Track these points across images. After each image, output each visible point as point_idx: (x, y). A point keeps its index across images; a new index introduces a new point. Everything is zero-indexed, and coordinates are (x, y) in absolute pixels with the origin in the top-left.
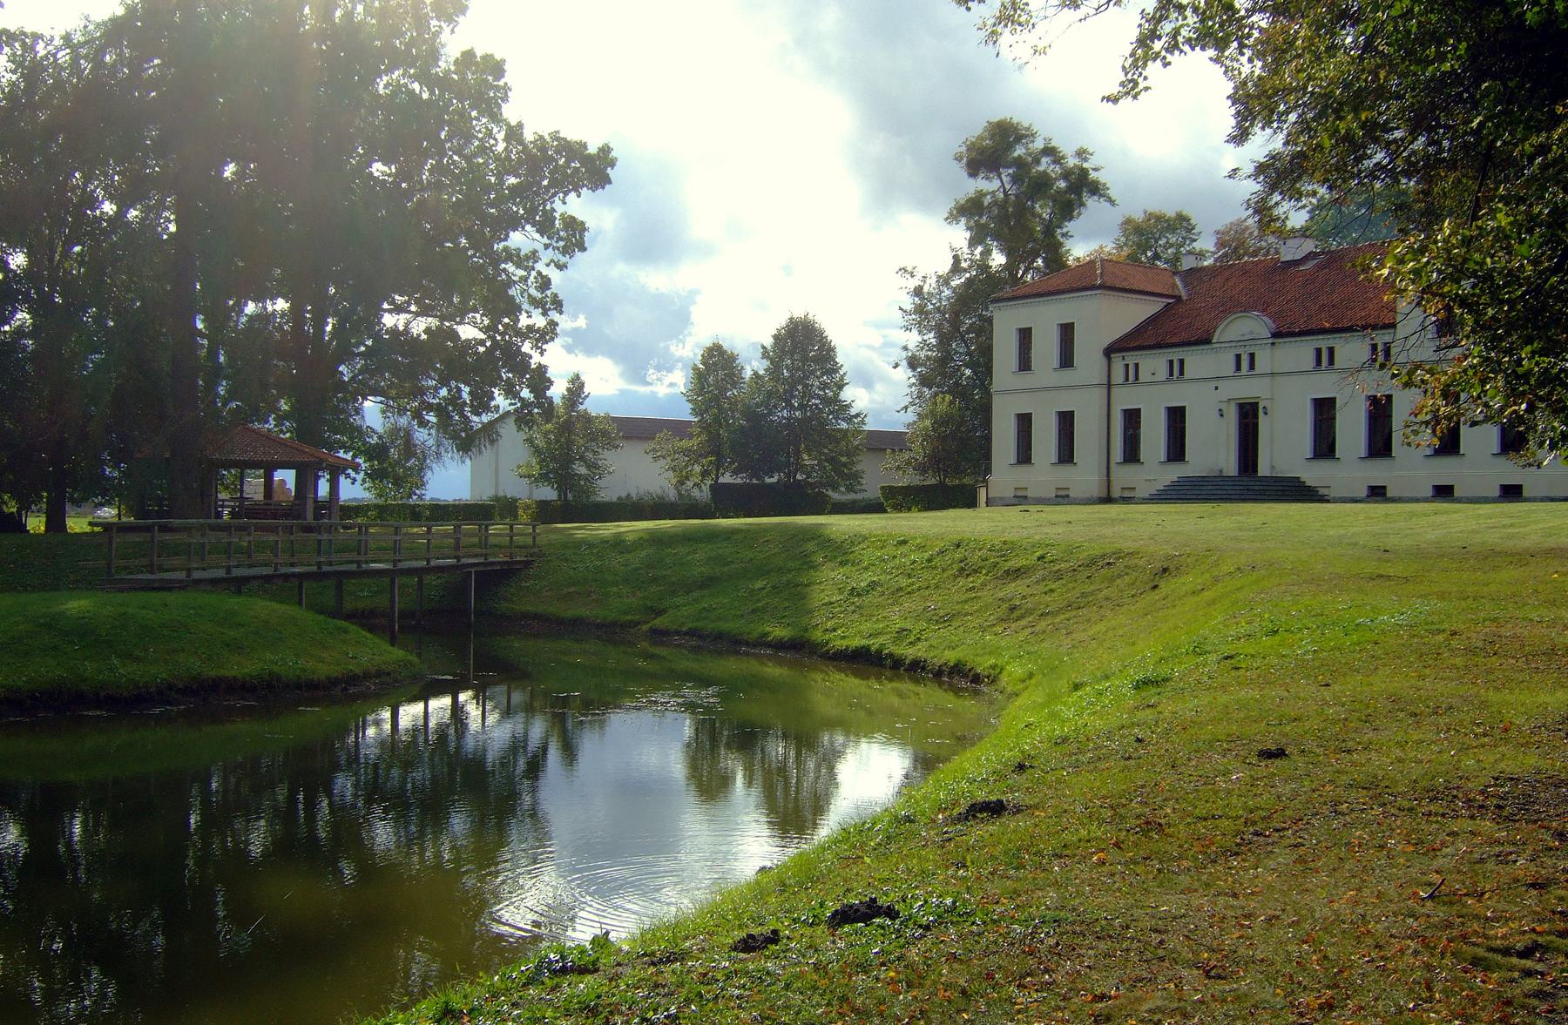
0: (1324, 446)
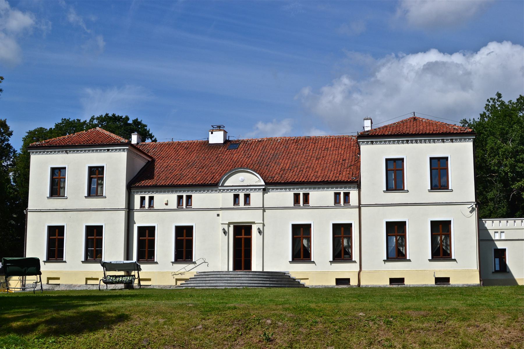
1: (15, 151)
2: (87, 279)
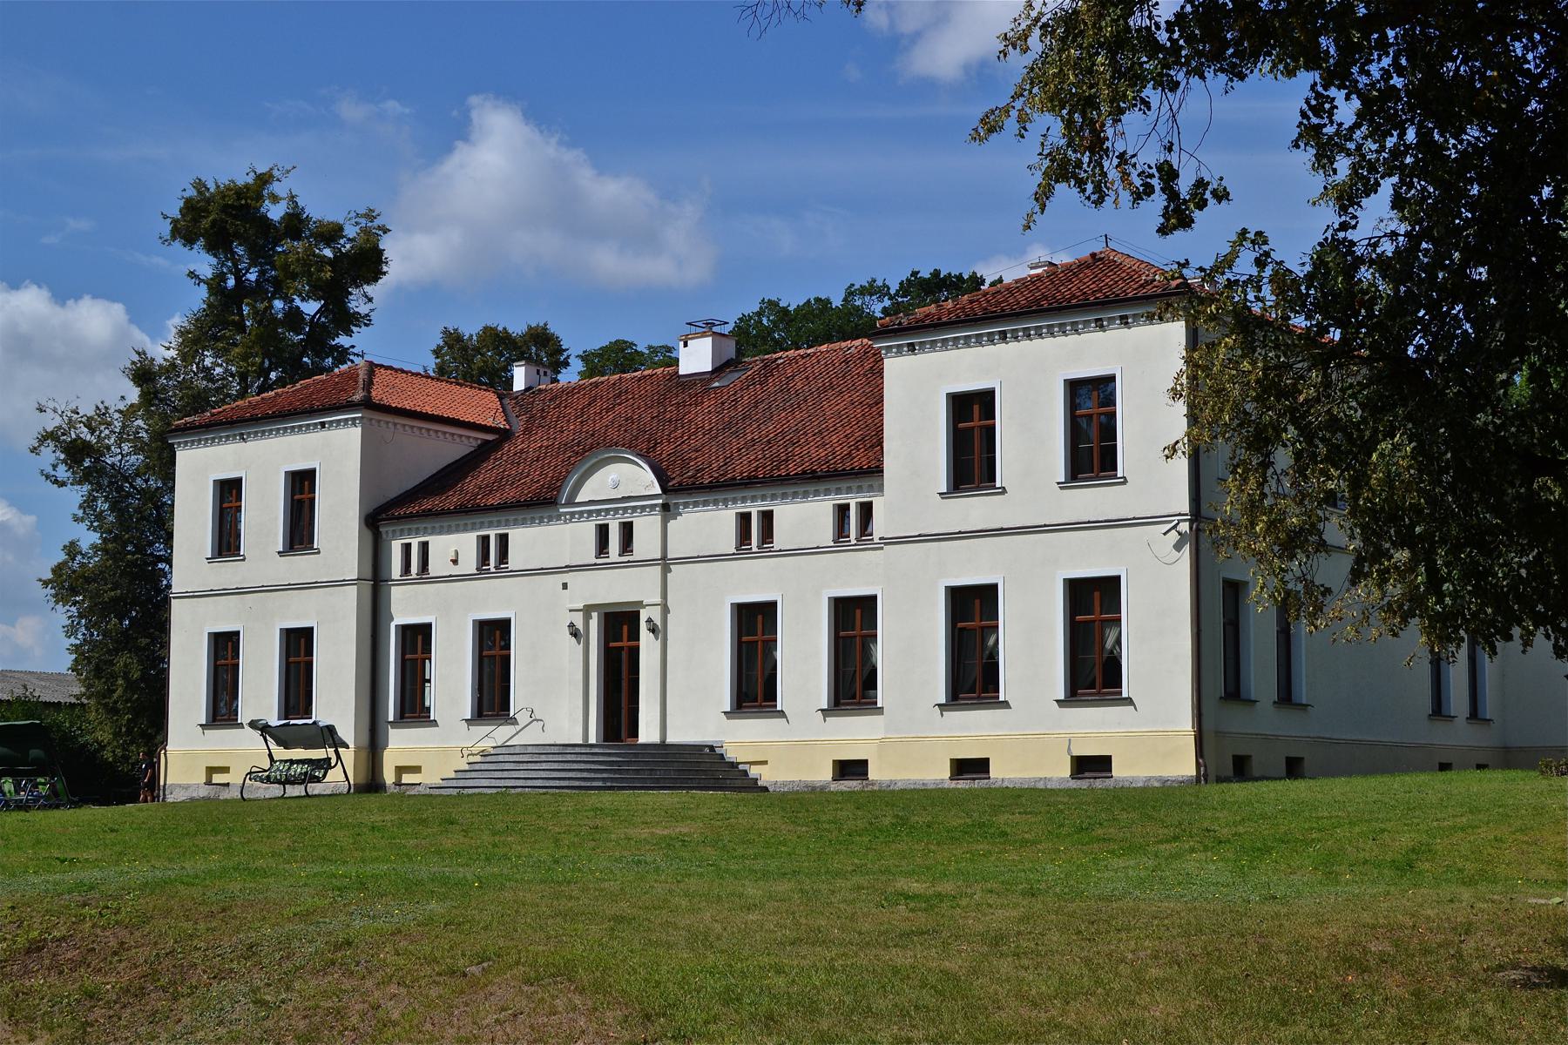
2: (211, 771)
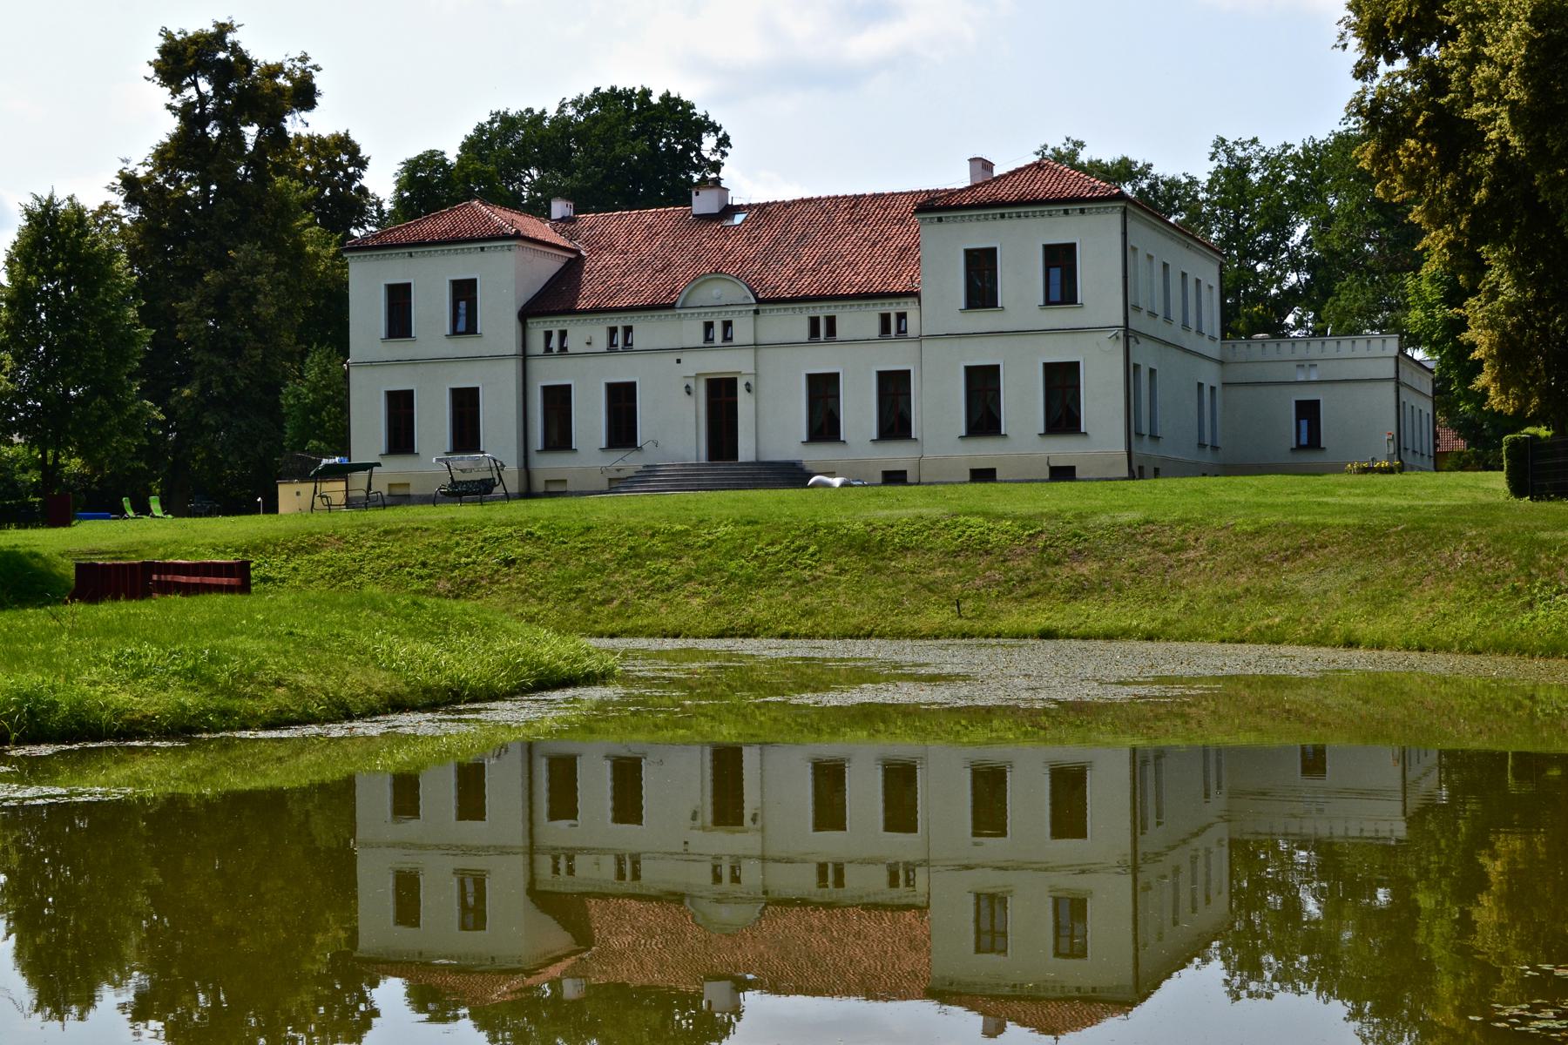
0: (824, 426)
1: (379, 204)
